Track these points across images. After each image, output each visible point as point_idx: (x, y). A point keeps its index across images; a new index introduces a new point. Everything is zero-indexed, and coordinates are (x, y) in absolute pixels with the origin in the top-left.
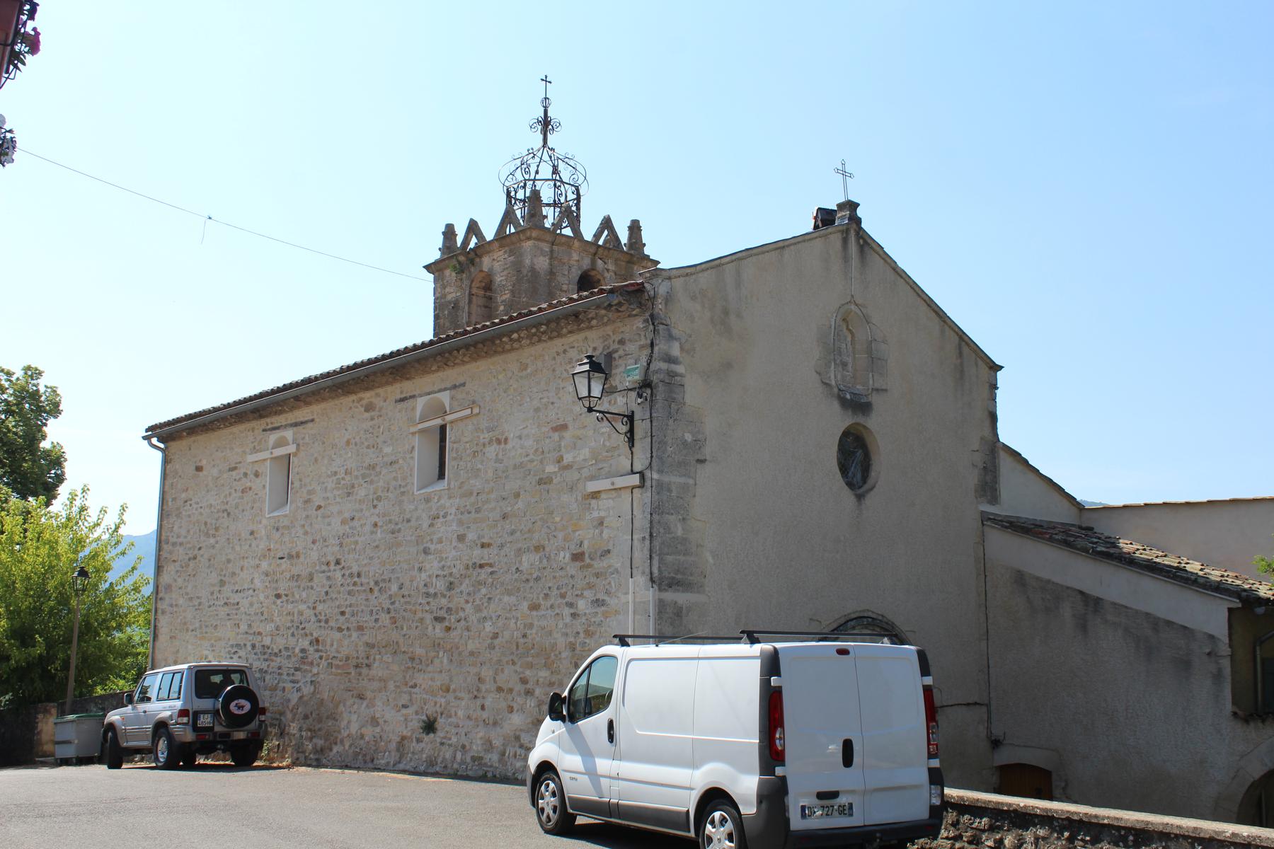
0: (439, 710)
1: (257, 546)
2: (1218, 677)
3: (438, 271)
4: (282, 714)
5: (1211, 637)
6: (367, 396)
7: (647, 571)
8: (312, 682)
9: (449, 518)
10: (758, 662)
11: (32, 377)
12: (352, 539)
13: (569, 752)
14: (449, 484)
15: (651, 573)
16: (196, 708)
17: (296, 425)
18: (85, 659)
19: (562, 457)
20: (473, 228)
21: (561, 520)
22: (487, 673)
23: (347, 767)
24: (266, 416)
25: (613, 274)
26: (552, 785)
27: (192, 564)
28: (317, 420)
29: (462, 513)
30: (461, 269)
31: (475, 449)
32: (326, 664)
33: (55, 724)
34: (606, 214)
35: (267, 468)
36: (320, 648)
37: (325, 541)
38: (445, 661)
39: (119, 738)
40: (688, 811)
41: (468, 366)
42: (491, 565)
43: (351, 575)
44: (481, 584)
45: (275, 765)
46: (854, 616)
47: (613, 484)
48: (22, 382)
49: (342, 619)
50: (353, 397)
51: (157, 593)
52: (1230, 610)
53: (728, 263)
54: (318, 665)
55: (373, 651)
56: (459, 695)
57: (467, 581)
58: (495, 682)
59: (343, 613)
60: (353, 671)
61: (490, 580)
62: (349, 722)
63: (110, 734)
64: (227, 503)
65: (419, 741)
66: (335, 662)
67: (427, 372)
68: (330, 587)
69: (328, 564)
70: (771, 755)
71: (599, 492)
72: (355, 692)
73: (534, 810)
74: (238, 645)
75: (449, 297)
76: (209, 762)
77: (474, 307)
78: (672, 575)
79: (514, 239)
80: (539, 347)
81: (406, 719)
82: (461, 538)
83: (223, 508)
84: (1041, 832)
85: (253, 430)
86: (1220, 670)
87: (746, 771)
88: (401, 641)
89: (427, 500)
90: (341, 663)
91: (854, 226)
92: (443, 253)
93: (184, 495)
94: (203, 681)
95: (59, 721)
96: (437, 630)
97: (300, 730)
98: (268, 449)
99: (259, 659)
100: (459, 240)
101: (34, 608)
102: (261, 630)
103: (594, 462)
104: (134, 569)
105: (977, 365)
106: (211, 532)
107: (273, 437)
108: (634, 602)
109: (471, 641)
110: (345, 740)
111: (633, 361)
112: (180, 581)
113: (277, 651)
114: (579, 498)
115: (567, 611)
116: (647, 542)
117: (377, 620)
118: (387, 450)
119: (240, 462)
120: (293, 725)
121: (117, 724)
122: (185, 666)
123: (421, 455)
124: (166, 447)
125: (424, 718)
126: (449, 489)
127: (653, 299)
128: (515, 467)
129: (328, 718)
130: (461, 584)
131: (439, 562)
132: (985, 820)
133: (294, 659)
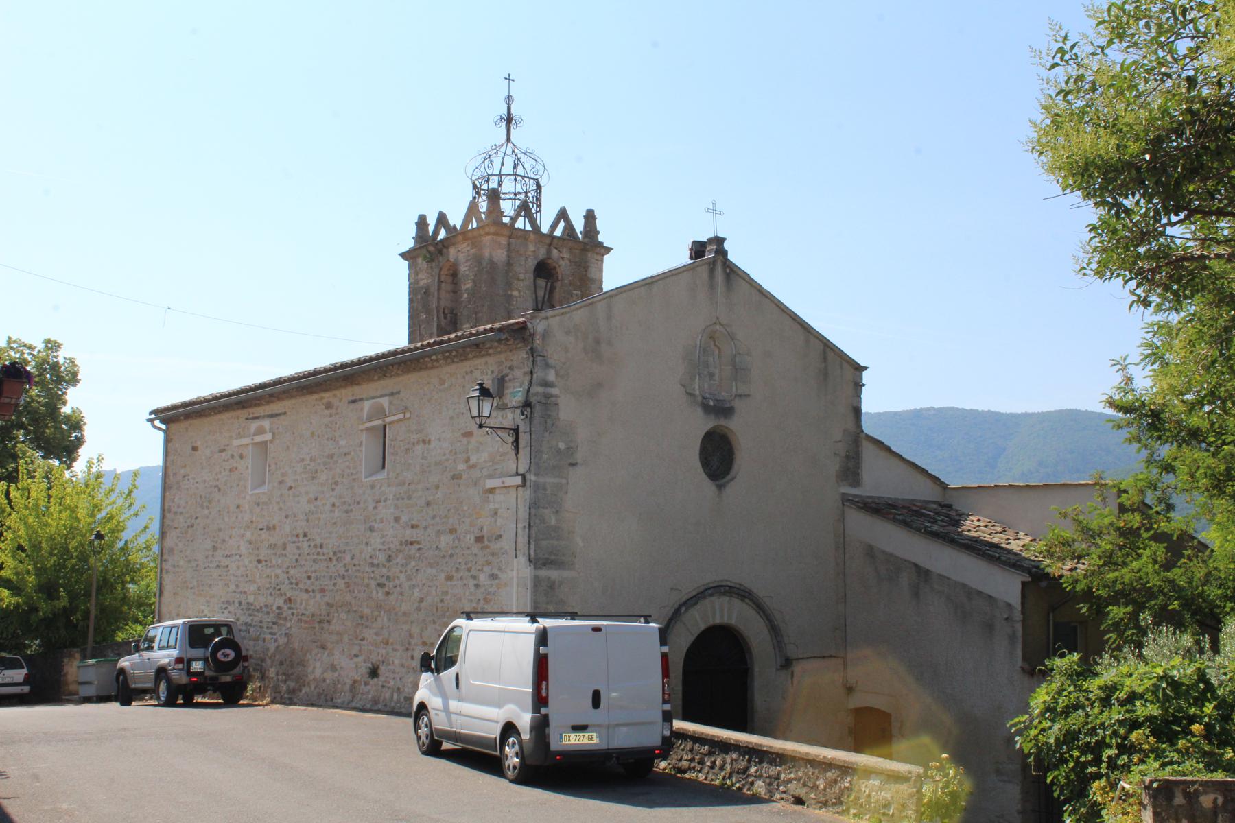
0: (381, 659)
1: (242, 518)
2: (1012, 638)
3: (411, 258)
4: (263, 660)
5: (1009, 605)
6: (327, 396)
7: (527, 552)
8: (286, 634)
9: (389, 502)
10: (533, 636)
11: (51, 349)
12: (316, 516)
13: (435, 695)
14: (388, 475)
15: (529, 555)
16: (189, 656)
17: (272, 416)
18: (103, 610)
19: (469, 458)
20: (442, 220)
21: (469, 508)
22: (415, 630)
23: (313, 705)
24: (246, 408)
25: (567, 262)
26: (426, 719)
27: (190, 531)
28: (288, 413)
29: (398, 499)
30: (431, 259)
31: (406, 447)
32: (297, 620)
33: (79, 667)
34: (562, 206)
35: (249, 452)
36: (292, 606)
37: (295, 516)
38: (385, 619)
39: (129, 681)
40: (496, 738)
41: (401, 378)
42: (418, 543)
43: (315, 546)
44: (410, 558)
45: (257, 703)
46: (712, 585)
47: (503, 482)
48: (43, 354)
49: (309, 582)
50: (316, 396)
51: (162, 555)
52: (1023, 584)
53: (600, 300)
54: (291, 620)
55: (333, 610)
56: (395, 647)
57: (401, 555)
58: (421, 637)
59: (309, 578)
60: (317, 625)
61: (418, 555)
62: (314, 668)
63: (121, 677)
64: (218, 480)
65: (366, 684)
66: (304, 618)
67: (371, 380)
68: (300, 555)
69: (297, 536)
70: (540, 700)
71: (495, 488)
72: (319, 643)
73: (415, 737)
74: (228, 602)
75: (422, 283)
76: (206, 700)
77: (443, 294)
78: (546, 556)
79: (475, 233)
80: (453, 366)
81: (357, 666)
82: (397, 519)
83: (215, 484)
84: (734, 756)
85: (238, 418)
86: (1014, 633)
87: (525, 711)
88: (353, 602)
89: (372, 487)
90: (308, 619)
91: (721, 258)
92: (416, 242)
93: (182, 471)
94: (196, 635)
95: (82, 664)
96: (380, 594)
97: (277, 674)
98: (250, 436)
99: (245, 614)
100: (431, 229)
101: (59, 564)
102: (246, 590)
103: (491, 464)
104: (146, 528)
105: (841, 367)
106: (205, 504)
107: (254, 426)
108: (518, 578)
109: (404, 604)
110: (311, 683)
111: (518, 384)
112: (181, 545)
113: (258, 607)
114: (481, 492)
115: (472, 582)
116: (527, 530)
117: (335, 584)
118: (342, 443)
119: (228, 445)
120: (272, 670)
121: (127, 669)
122: (180, 622)
123: (366, 450)
124: (167, 428)
125: (370, 665)
126: (388, 479)
127: (532, 335)
128: (437, 464)
129: (298, 664)
130: (397, 557)
131: (381, 538)
132: (707, 747)
133: (272, 615)
